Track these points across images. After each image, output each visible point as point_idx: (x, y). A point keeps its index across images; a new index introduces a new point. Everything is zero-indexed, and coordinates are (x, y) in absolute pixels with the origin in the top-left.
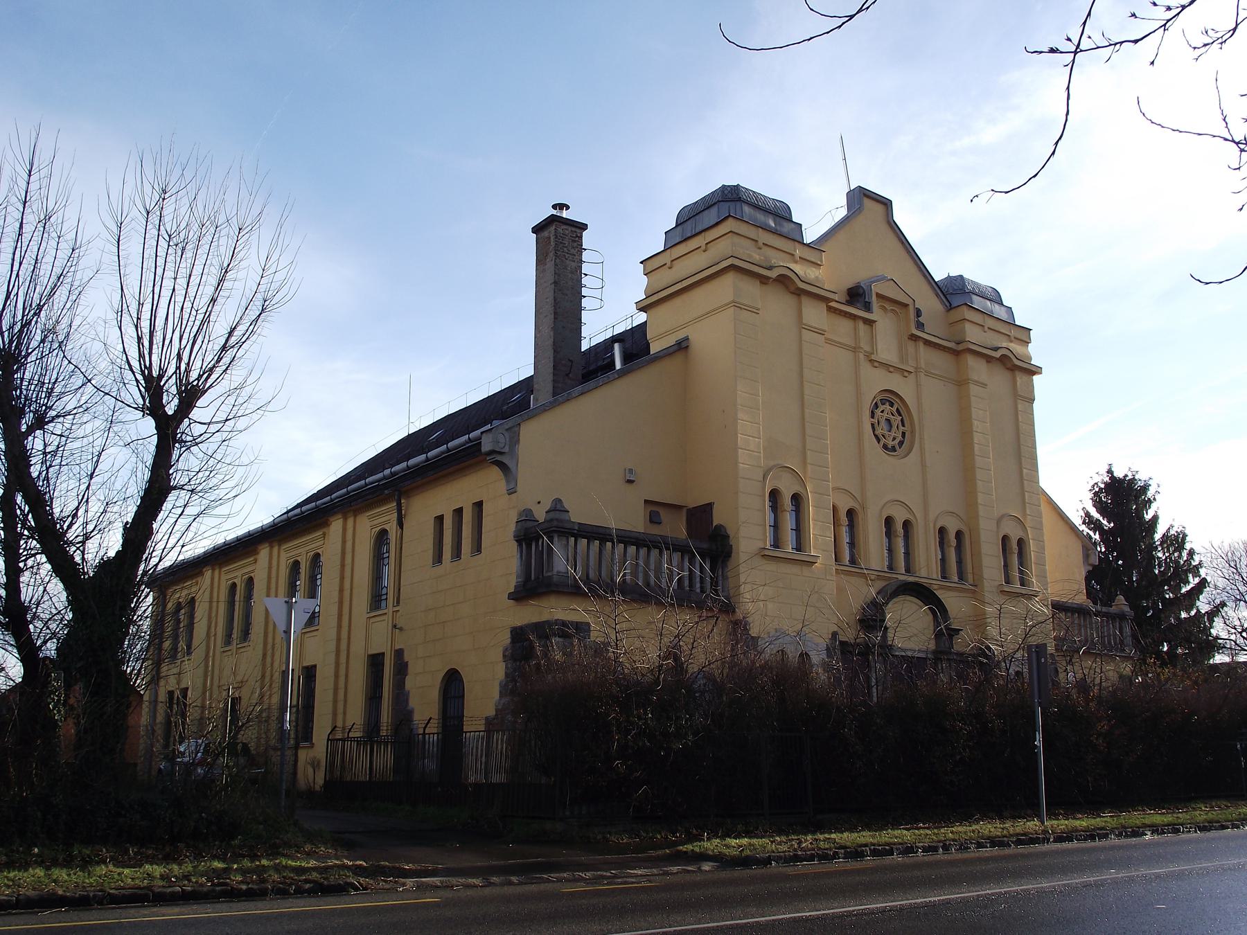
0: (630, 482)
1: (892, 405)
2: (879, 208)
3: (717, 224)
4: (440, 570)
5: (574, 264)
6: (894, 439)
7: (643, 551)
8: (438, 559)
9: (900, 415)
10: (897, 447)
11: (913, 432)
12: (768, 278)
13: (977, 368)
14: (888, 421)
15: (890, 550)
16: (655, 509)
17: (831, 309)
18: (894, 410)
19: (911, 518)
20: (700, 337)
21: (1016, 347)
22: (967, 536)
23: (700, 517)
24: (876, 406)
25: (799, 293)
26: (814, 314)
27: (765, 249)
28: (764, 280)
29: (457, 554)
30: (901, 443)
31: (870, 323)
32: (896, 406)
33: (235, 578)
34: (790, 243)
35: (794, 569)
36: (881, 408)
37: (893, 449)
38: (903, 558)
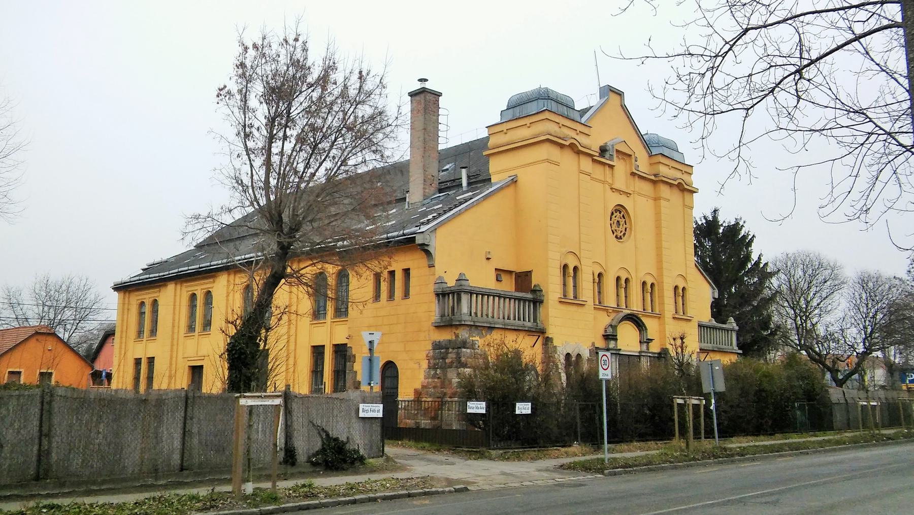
0: (488, 259)
1: (620, 213)
2: (617, 98)
3: (537, 113)
4: (377, 305)
5: (435, 118)
6: (621, 232)
7: (502, 300)
8: (377, 297)
9: (624, 218)
10: (622, 237)
11: (631, 229)
12: (564, 145)
13: (664, 191)
14: (618, 221)
15: (565, 285)
16: (500, 273)
17: (594, 161)
18: (621, 215)
19: (603, 271)
20: (524, 177)
21: (685, 177)
22: (656, 286)
23: (523, 279)
24: (612, 214)
25: (579, 153)
26: (586, 164)
27: (563, 127)
28: (562, 146)
29: (391, 296)
30: (624, 234)
31: (611, 167)
32: (622, 213)
33: (145, 299)
34: (576, 124)
35: (573, 309)
36: (615, 214)
37: (621, 238)
38: (572, 289)
